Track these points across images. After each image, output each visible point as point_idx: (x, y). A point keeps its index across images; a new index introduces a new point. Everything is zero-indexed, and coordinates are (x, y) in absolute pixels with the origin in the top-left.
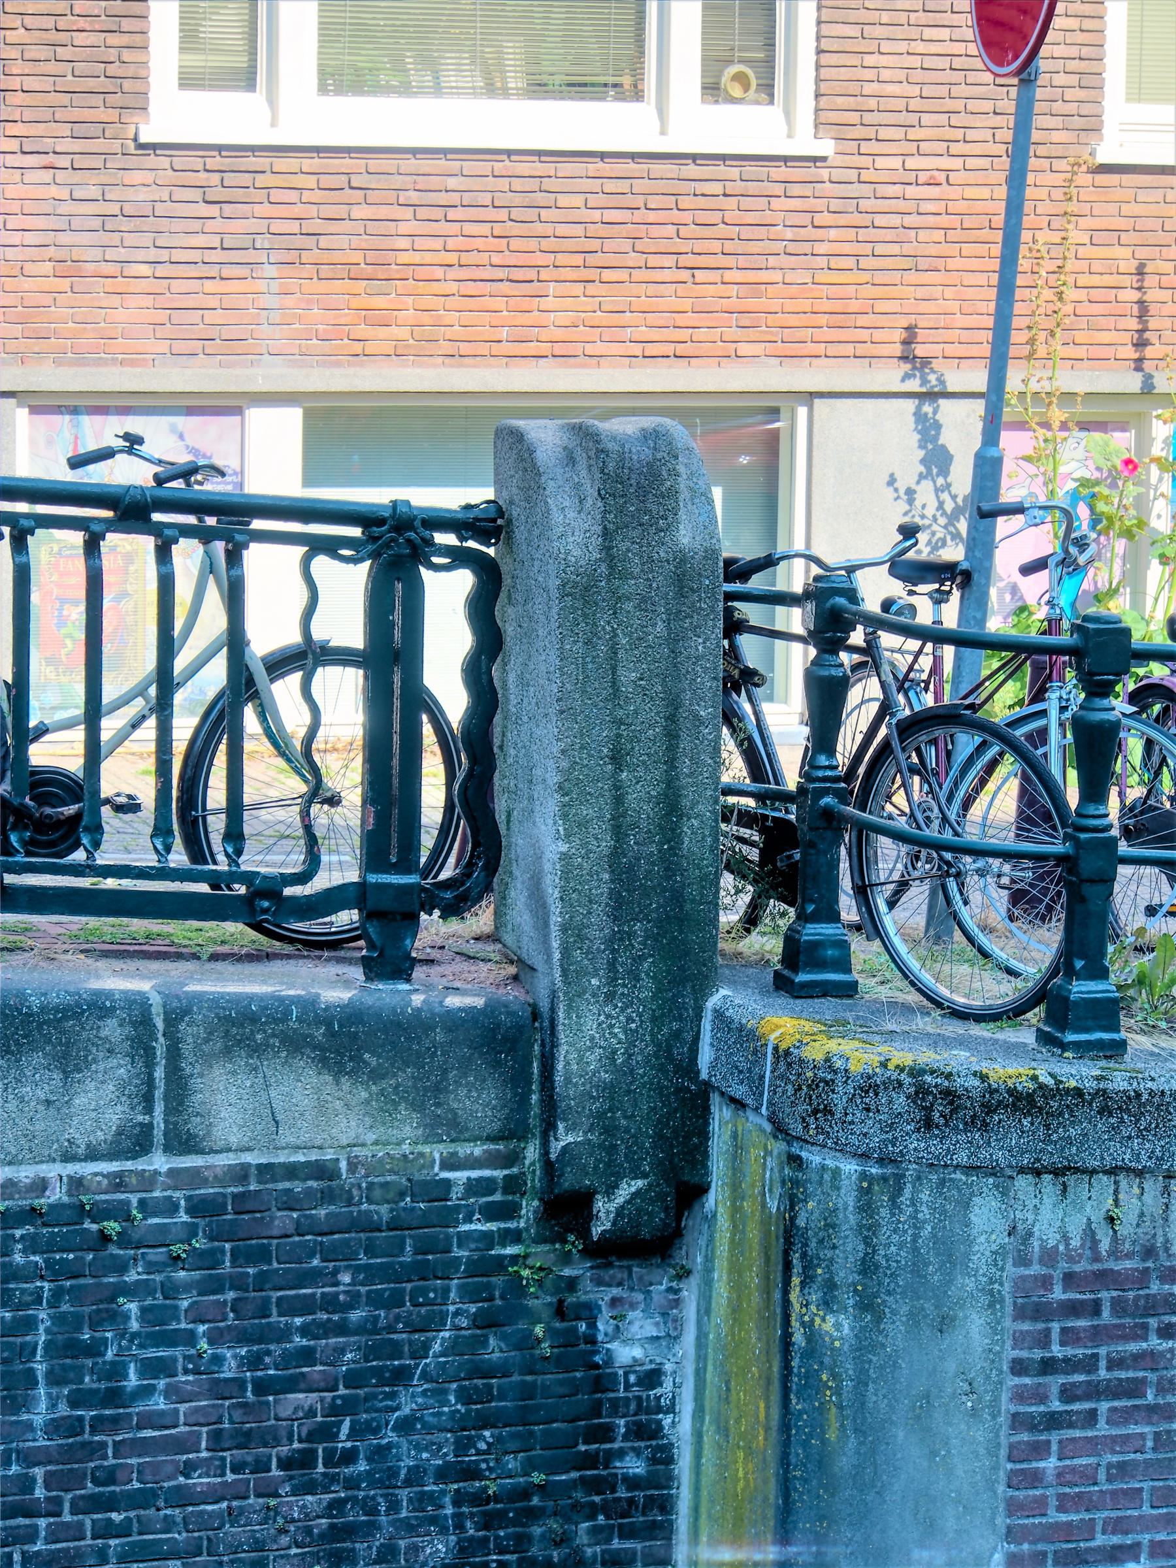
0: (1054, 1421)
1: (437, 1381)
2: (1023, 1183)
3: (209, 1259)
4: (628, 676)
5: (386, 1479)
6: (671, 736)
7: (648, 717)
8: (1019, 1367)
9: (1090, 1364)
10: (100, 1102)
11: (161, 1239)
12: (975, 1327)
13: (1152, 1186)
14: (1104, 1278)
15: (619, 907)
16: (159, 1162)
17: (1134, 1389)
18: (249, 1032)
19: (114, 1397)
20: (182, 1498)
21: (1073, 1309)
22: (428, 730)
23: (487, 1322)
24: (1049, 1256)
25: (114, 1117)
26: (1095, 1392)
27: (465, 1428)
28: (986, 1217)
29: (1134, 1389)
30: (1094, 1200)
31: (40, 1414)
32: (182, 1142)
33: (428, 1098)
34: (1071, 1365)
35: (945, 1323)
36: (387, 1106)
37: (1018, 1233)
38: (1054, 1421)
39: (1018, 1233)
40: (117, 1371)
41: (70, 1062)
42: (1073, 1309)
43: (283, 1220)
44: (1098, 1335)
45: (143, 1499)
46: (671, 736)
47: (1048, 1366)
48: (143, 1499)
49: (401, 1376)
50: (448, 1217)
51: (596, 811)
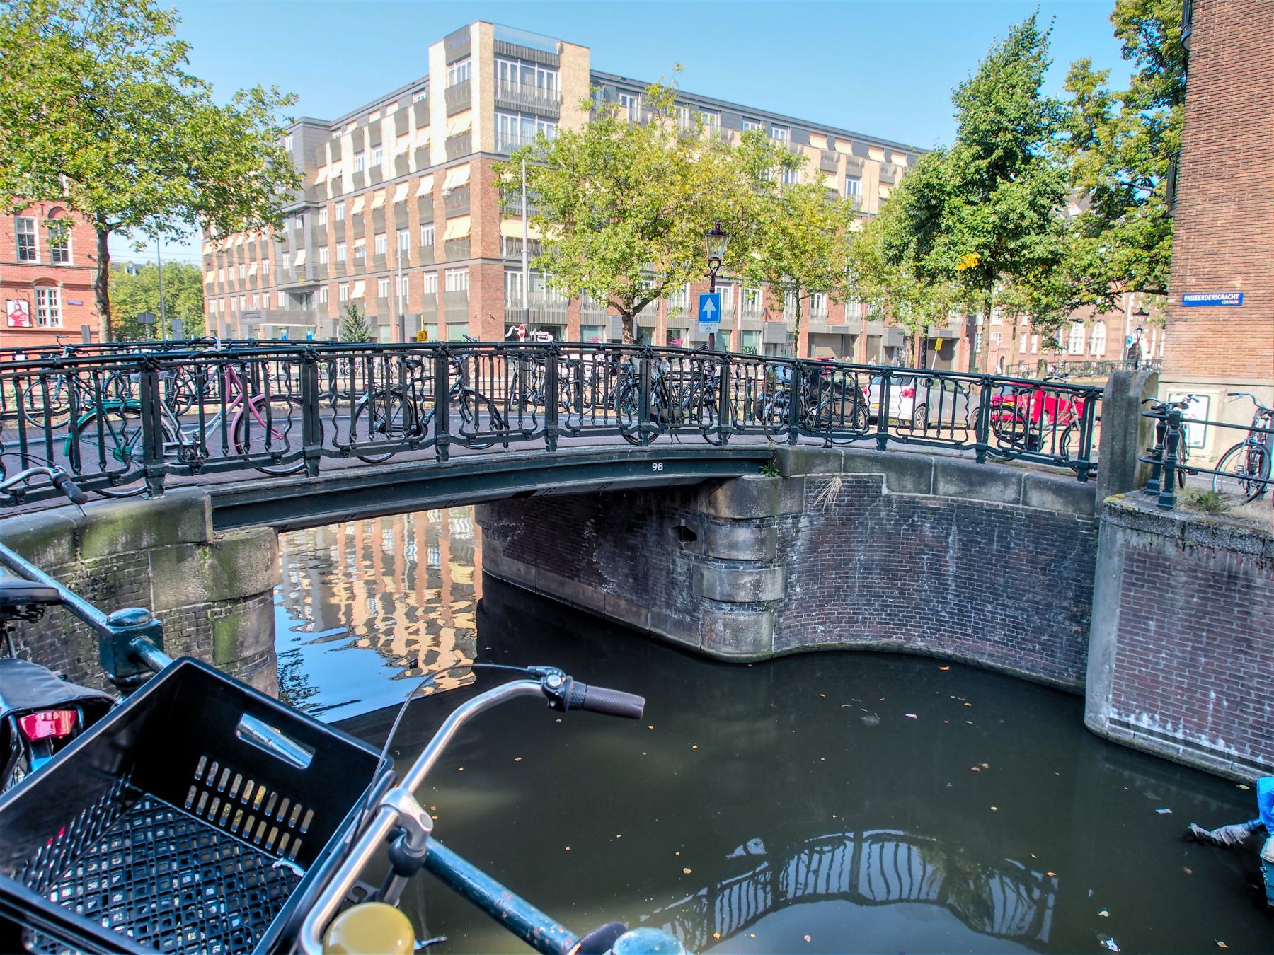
0: (1133, 584)
1: (1073, 561)
2: (1128, 531)
3: (1028, 526)
4: (1116, 422)
5: (1061, 578)
6: (1125, 436)
7: (1120, 432)
8: (1125, 571)
9: (1143, 574)
10: (1011, 493)
11: (1019, 520)
12: (1116, 559)
13: (1161, 539)
14: (1147, 556)
15: (1112, 470)
16: (1021, 506)
17: (1154, 583)
18: (1040, 485)
19: (1008, 547)
20: (1020, 570)
21: (1140, 561)
22: (385, 456)
23: (1085, 551)
24: (1134, 548)
25: (1013, 496)
26: (1144, 581)
27: (1078, 572)
28: (1120, 536)
29: (1154, 583)
30: (1146, 539)
31: (995, 547)
32: (1025, 503)
33: (1075, 503)
34: (1137, 573)
35: (1110, 557)
36: (1066, 504)
37: (1127, 543)
38: (1133, 584)
39: (1127, 543)
40: (1009, 543)
41: (1006, 484)
42: (1140, 561)
43: (1044, 522)
44: (1145, 568)
45: (1013, 568)
46: (1125, 436)
47: (1132, 572)
48: (1013, 568)
49: (1065, 558)
50: (1078, 529)
51: (1108, 450)
